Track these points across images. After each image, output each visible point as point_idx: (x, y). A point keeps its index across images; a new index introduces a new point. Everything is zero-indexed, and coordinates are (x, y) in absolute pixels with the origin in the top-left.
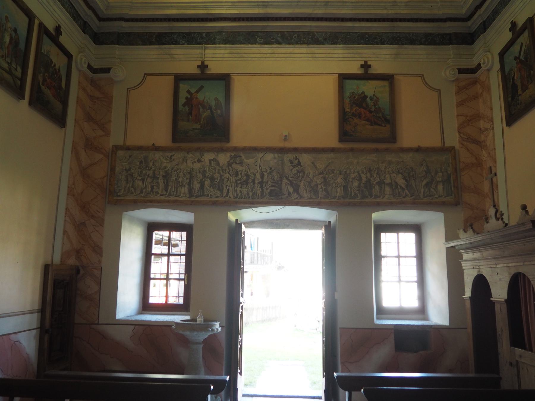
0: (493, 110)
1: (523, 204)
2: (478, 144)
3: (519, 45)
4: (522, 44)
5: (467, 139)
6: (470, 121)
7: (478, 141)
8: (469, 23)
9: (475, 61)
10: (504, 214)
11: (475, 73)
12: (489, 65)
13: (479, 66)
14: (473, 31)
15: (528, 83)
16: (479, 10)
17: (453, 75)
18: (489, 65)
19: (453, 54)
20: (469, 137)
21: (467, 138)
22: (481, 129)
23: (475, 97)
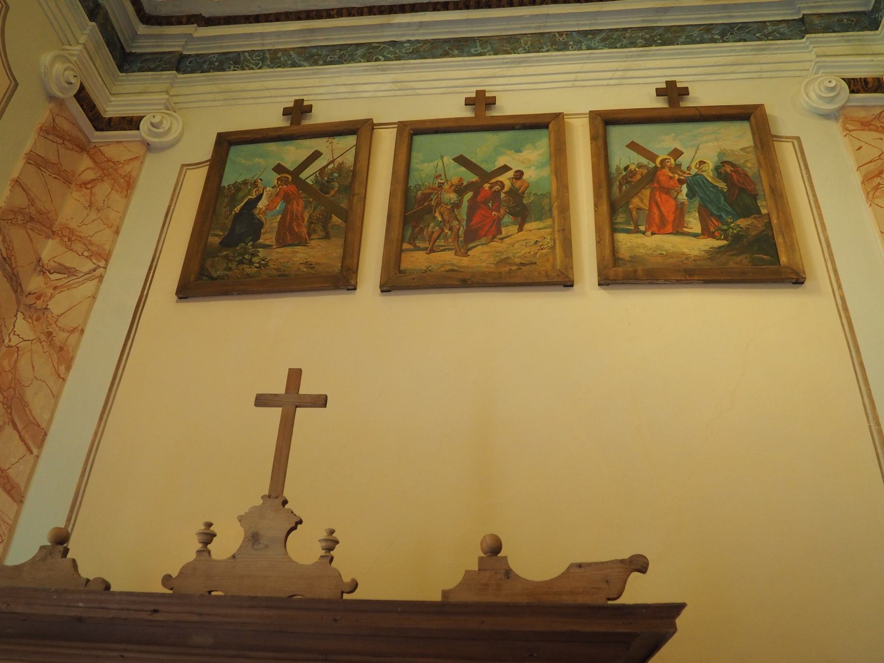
0: (120, 236)
1: (53, 529)
2: (16, 292)
3: (306, 154)
4: (316, 155)
5: (4, 259)
6: (32, 219)
7: (20, 285)
8: (142, 29)
9: (114, 106)
10: (337, 542)
11: (97, 129)
12: (156, 140)
13: (133, 123)
14: (133, 51)
15: (309, 234)
16: (195, 25)
17: (67, 86)
18: (156, 140)
19: (84, 44)
20: (10, 259)
21: (5, 256)
22: (39, 260)
23: (67, 179)
